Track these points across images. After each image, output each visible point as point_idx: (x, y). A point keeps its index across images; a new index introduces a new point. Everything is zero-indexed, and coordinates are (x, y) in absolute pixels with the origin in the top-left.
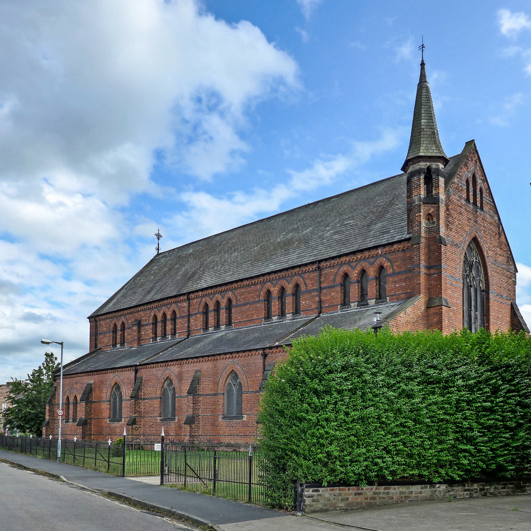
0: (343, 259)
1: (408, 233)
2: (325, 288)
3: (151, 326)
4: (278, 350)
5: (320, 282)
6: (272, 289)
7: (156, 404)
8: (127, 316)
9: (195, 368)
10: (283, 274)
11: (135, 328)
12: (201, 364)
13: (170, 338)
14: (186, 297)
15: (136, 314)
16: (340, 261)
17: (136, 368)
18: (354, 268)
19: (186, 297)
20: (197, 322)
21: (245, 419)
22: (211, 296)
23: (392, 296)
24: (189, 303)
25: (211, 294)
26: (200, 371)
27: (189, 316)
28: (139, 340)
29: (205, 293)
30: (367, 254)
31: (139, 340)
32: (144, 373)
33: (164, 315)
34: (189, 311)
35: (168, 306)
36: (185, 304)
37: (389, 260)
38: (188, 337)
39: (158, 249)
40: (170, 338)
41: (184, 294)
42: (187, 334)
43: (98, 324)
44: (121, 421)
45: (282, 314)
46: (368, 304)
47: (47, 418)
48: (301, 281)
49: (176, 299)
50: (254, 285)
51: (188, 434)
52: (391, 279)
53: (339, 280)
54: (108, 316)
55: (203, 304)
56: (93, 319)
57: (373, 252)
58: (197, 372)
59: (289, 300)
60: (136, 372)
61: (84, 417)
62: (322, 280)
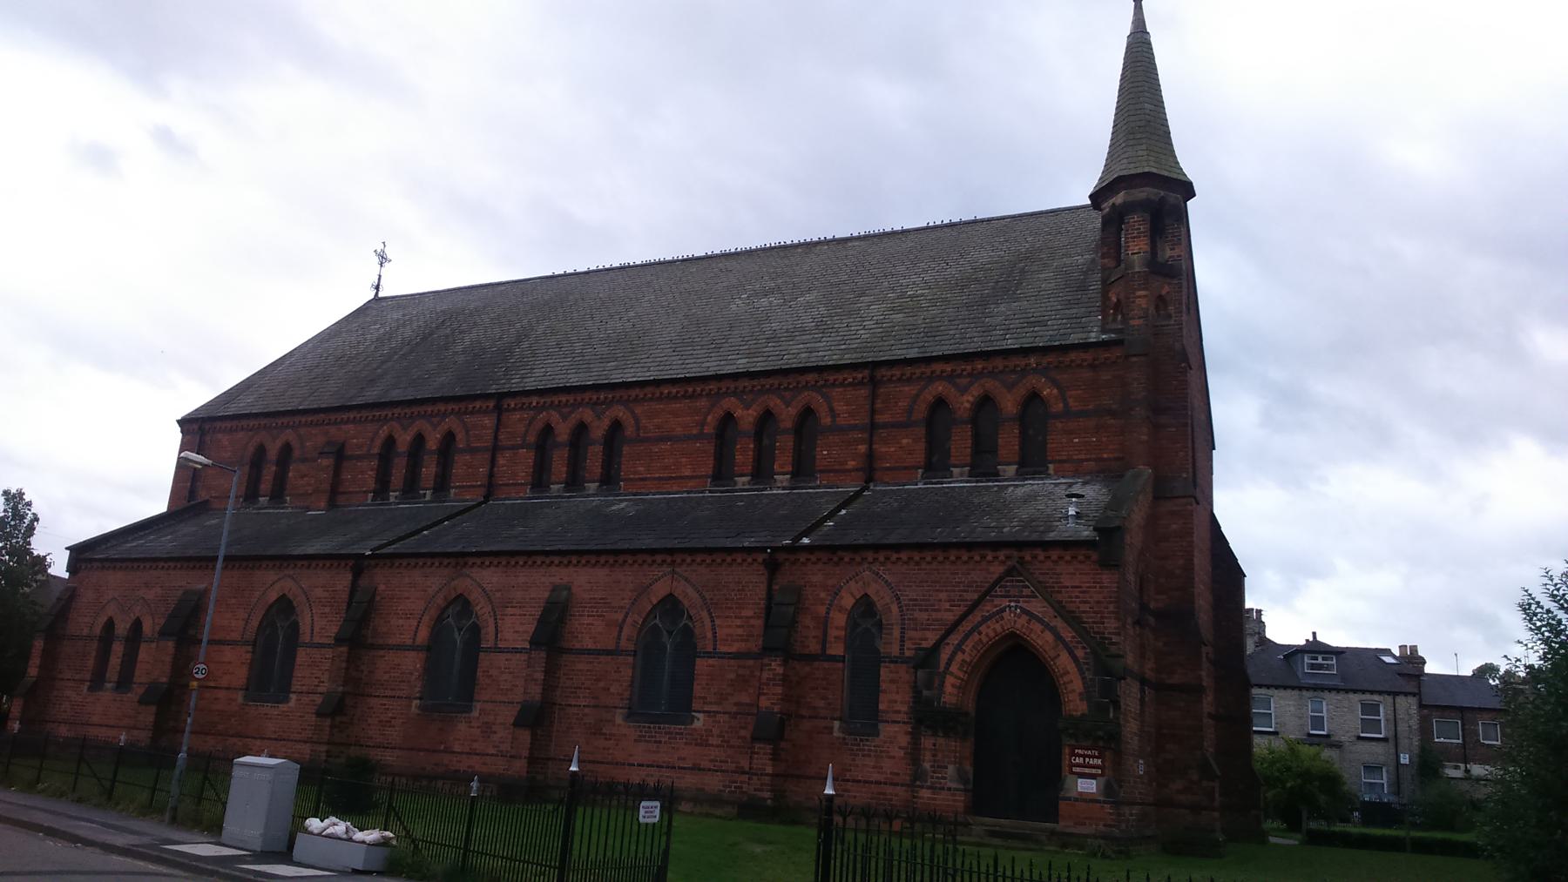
0: (938, 367)
1: (1104, 331)
2: (885, 426)
3: (375, 463)
4: (813, 558)
5: (873, 412)
6: (738, 413)
7: (412, 663)
8: (302, 431)
9: (553, 579)
10: (775, 381)
11: (326, 462)
12: (571, 569)
13: (428, 498)
14: (491, 404)
15: (333, 430)
16: (928, 371)
17: (358, 565)
18: (964, 390)
19: (491, 404)
20: (517, 466)
21: (698, 724)
22: (565, 410)
23: (1061, 462)
24: (499, 420)
25: (566, 405)
26: (569, 589)
27: (495, 449)
28: (335, 493)
29: (831, 378)
30: (999, 363)
31: (335, 493)
32: (382, 580)
33: (420, 439)
34: (496, 438)
35: (435, 420)
36: (488, 421)
37: (1055, 383)
38: (487, 498)
39: (377, 288)
40: (428, 498)
41: (487, 397)
42: (483, 491)
43: (208, 438)
44: (286, 700)
45: (762, 474)
46: (997, 474)
47: (33, 671)
48: (818, 401)
49: (462, 406)
50: (691, 397)
51: (525, 753)
52: (1059, 425)
53: (921, 411)
54: (244, 423)
55: (539, 425)
56: (196, 427)
57: (1020, 362)
58: (555, 589)
59: (784, 447)
60: (357, 573)
61: (164, 680)
62: (879, 405)
